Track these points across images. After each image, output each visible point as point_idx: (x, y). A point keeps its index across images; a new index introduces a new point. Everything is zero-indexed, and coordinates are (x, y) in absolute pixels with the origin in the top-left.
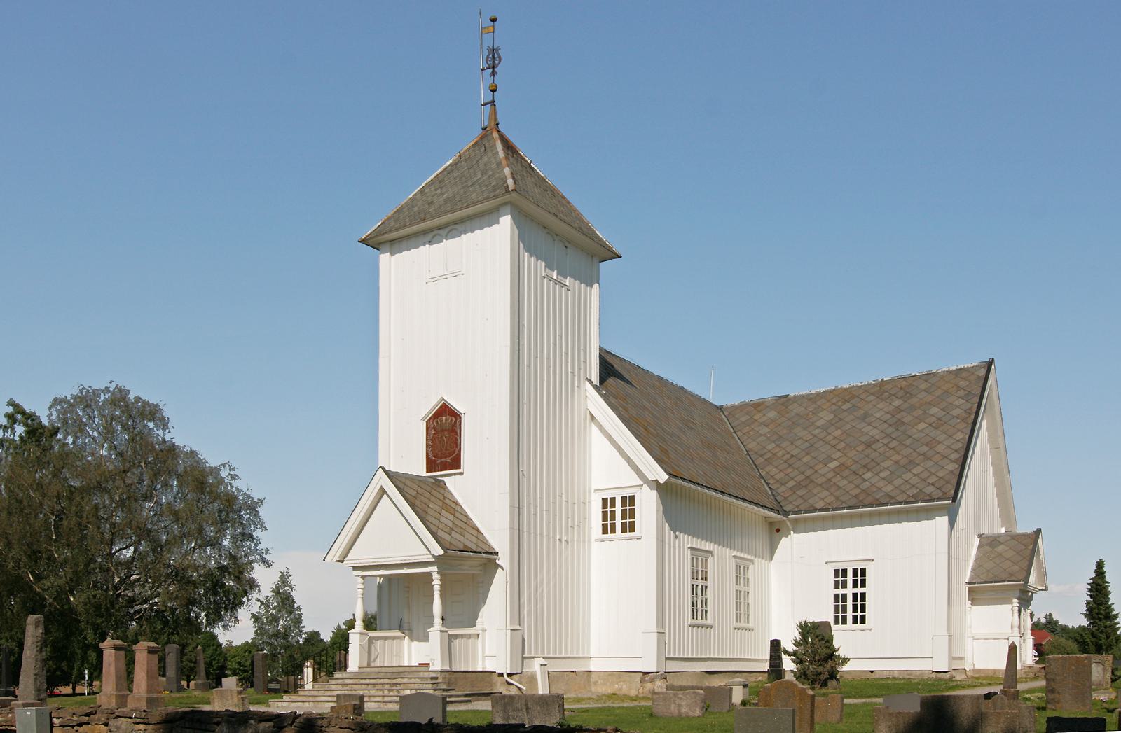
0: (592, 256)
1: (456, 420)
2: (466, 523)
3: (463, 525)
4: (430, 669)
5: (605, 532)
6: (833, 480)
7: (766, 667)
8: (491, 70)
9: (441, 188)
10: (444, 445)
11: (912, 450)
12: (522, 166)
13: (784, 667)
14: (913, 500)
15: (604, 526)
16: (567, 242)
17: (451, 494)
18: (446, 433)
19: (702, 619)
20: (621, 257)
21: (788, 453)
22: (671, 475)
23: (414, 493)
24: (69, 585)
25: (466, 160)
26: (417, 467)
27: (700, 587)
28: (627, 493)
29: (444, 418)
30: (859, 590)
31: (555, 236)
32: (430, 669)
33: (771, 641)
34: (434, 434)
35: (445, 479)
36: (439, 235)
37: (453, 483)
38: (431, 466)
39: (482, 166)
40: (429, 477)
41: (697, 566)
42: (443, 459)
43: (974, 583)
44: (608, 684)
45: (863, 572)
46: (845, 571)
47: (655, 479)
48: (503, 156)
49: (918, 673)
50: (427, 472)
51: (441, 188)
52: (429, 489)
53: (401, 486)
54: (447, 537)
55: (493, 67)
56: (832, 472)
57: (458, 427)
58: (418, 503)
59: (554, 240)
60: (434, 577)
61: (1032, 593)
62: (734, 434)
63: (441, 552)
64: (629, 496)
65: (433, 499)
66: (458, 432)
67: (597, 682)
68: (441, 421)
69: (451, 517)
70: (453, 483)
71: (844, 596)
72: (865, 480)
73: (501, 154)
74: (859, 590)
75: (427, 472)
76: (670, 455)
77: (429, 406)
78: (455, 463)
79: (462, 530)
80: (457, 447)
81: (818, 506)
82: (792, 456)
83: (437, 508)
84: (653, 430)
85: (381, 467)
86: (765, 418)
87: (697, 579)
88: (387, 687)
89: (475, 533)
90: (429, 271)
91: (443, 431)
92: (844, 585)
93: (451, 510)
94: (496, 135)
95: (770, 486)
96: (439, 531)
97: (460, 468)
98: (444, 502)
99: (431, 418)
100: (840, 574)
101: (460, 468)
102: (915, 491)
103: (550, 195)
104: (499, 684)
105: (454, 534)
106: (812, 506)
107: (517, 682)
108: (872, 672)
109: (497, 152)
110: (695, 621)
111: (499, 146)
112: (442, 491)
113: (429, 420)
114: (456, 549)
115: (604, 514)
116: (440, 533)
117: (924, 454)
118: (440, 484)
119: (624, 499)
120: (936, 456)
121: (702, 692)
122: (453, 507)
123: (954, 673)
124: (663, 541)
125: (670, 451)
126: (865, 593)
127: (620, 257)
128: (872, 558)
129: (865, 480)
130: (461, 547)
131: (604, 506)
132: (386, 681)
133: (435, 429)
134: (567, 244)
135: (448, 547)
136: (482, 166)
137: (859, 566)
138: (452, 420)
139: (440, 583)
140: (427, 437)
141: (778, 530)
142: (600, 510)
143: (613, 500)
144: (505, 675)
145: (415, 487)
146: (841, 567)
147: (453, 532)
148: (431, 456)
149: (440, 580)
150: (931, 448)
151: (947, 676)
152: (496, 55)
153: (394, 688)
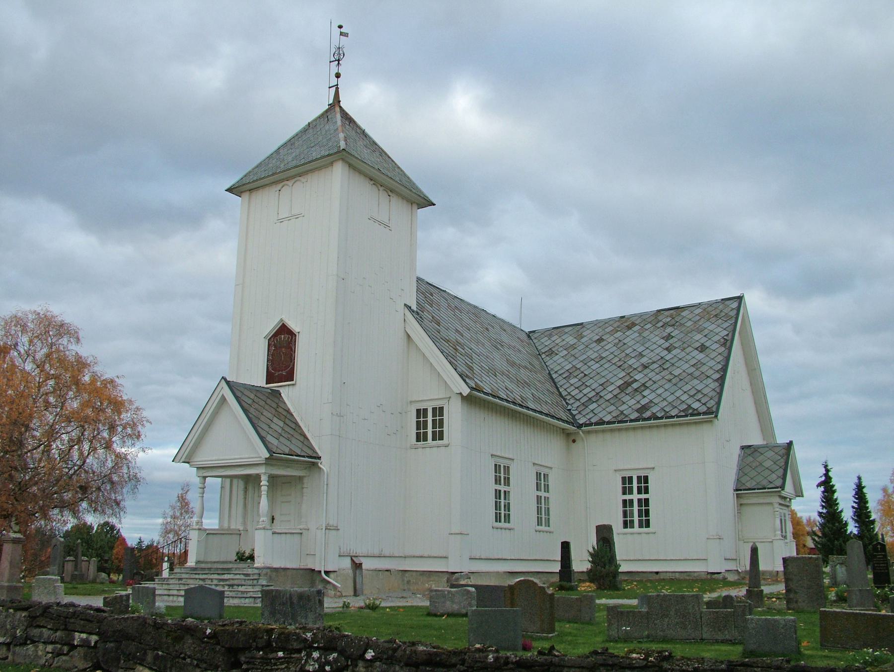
0: (412, 204)
1: (292, 339)
2: (294, 430)
3: (292, 432)
4: (256, 565)
5: (418, 440)
6: (618, 396)
7: (557, 568)
8: (337, 62)
9: (292, 149)
10: (281, 360)
11: (577, 341)
12: (356, 132)
13: (573, 568)
14: (684, 414)
15: (418, 435)
16: (390, 191)
17: (285, 403)
18: (283, 349)
19: (505, 522)
20: (435, 205)
21: (582, 372)
22: (472, 388)
23: (250, 402)
24: (72, 500)
25: (313, 128)
26: (258, 378)
27: (543, 498)
28: (437, 404)
29: (283, 336)
30: (643, 496)
31: (380, 186)
32: (256, 565)
33: (562, 543)
34: (274, 350)
35: (282, 390)
36: (287, 185)
37: (287, 393)
38: (270, 379)
39: (324, 132)
40: (268, 388)
41: (500, 473)
42: (280, 372)
43: (741, 490)
44: (420, 583)
45: (646, 479)
46: (631, 479)
47: (459, 392)
48: (340, 124)
49: (696, 574)
50: (266, 384)
51: (292, 149)
52: (264, 398)
53: (239, 394)
54: (275, 442)
55: (339, 60)
56: (618, 389)
57: (293, 343)
58: (252, 410)
59: (379, 190)
60: (262, 479)
61: (790, 499)
62: (539, 356)
63: (813, 546)
64: (439, 408)
65: (267, 407)
66: (293, 349)
67: (410, 581)
68: (281, 339)
69: (281, 424)
70: (287, 393)
71: (631, 501)
72: (644, 397)
73: (339, 123)
74: (643, 496)
75: (266, 384)
76: (475, 371)
77: (270, 326)
78: (290, 376)
79: (289, 436)
80: (291, 362)
81: (606, 419)
82: (585, 375)
83: (270, 415)
84: (461, 350)
85: (223, 378)
86: (565, 342)
87: (540, 491)
88: (215, 582)
89: (302, 438)
90: (278, 213)
91: (281, 347)
92: (631, 492)
93: (283, 417)
94: (338, 109)
95: (567, 401)
96: (269, 436)
97: (293, 380)
98: (276, 411)
99: (272, 337)
100: (627, 481)
101: (293, 380)
102: (684, 406)
103: (378, 155)
104: (317, 582)
105: (282, 439)
106: (601, 419)
107: (334, 580)
108: (657, 573)
109: (336, 122)
110: (540, 528)
111: (338, 116)
112: (277, 401)
113: (270, 338)
114: (306, 455)
115: (418, 423)
116: (269, 438)
117: (691, 374)
118: (276, 394)
119: (434, 409)
120: (702, 376)
121: (473, 589)
122: (287, 416)
123: (727, 575)
124: (768, 503)
125: (474, 368)
126: (648, 499)
127: (434, 205)
128: (652, 466)
129: (644, 397)
130: (287, 451)
131: (418, 416)
132: (216, 576)
133: (275, 346)
134: (390, 193)
135: (274, 451)
136: (324, 132)
137: (642, 474)
138: (289, 338)
139: (267, 484)
140: (268, 353)
141: (574, 441)
142: (414, 420)
143: (425, 410)
144: (323, 573)
145: (252, 396)
146: (627, 474)
147: (281, 437)
148: (270, 369)
149: (268, 482)
150: (697, 369)
151: (721, 576)
152: (341, 52)
153: (222, 583)
